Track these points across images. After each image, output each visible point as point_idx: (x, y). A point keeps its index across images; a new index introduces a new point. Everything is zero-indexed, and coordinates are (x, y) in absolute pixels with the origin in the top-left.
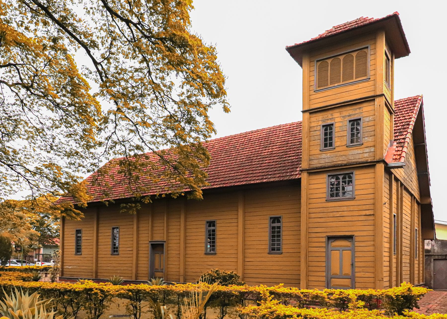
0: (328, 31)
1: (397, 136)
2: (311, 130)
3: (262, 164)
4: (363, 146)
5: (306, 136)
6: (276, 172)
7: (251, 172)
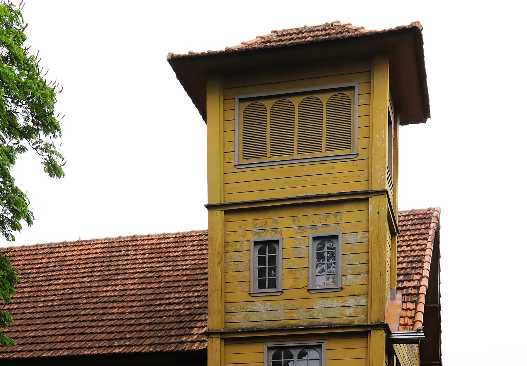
0: (262, 38)
1: (402, 281)
2: (229, 248)
3: (103, 314)
4: (342, 293)
5: (217, 261)
6: (142, 334)
7: (79, 331)
